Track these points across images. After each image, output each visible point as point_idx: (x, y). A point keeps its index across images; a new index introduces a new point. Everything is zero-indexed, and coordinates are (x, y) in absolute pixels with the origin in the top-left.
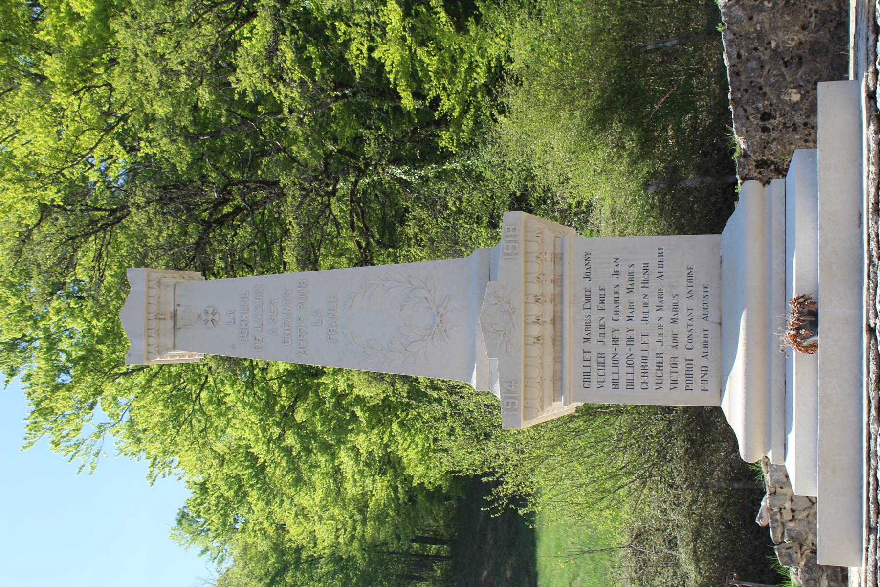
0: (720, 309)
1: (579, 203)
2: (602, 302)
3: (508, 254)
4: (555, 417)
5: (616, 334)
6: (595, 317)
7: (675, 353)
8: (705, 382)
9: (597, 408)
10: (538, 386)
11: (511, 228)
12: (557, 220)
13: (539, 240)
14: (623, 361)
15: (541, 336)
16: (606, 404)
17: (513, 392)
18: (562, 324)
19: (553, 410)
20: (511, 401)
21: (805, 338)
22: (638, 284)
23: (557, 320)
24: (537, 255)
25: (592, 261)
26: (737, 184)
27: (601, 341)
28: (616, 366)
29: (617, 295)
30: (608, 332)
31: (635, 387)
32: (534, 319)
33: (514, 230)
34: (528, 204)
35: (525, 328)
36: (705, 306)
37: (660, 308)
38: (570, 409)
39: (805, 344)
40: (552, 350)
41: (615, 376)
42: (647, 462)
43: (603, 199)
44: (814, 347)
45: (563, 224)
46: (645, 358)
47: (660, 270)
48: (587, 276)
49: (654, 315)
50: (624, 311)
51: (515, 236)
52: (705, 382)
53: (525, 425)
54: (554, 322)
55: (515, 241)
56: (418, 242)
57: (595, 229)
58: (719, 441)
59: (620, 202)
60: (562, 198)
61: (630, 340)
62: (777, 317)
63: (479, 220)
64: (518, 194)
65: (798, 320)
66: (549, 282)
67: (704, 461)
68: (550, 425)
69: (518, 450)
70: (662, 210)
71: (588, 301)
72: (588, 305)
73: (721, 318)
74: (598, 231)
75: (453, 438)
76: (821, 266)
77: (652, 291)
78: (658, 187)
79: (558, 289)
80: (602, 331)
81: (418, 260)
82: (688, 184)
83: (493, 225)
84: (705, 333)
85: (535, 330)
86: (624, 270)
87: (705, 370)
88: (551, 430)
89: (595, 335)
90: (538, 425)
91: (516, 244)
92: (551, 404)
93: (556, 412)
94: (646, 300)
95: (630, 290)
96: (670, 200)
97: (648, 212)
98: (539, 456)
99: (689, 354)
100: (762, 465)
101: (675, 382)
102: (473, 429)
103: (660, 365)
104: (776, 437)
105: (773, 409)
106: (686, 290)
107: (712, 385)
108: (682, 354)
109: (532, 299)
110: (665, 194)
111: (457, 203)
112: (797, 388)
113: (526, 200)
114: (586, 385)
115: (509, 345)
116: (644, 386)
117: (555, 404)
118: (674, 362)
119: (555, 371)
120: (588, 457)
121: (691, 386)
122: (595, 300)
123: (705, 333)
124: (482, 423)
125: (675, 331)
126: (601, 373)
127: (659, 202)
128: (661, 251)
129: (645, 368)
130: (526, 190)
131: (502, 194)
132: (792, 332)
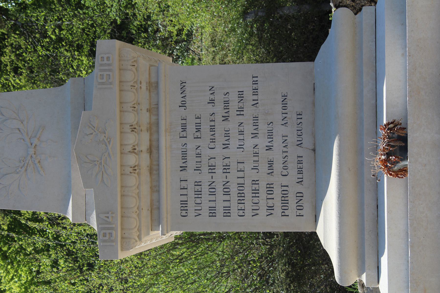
0: (314, 135)
1: (180, 32)
2: (198, 130)
3: (103, 83)
4: (158, 245)
5: (212, 162)
6: (191, 145)
7: (271, 179)
8: (300, 208)
9: (200, 235)
10: (135, 216)
11: (105, 56)
12: (158, 49)
13: (134, 69)
14: (220, 189)
15: (138, 165)
16: (209, 231)
17: (110, 223)
18: (158, 153)
19: (152, 240)
20: (107, 232)
21: (394, 163)
22: (233, 112)
23: (153, 149)
24: (132, 83)
25: (188, 89)
26: (331, 12)
27: (198, 169)
28: (212, 194)
29: (212, 123)
30: (205, 160)
31: (232, 214)
32: (130, 148)
33: (108, 58)
34: (129, 33)
35: (121, 158)
36: (299, 133)
37: (255, 136)
38: (170, 237)
39: (396, 168)
40: (149, 179)
41: (212, 204)
42: (250, 286)
43: (203, 27)
44: (404, 171)
45: (165, 53)
46: (241, 185)
47: (255, 97)
48: (183, 105)
49: (249, 143)
50: (220, 139)
51: (109, 65)
52: (300, 208)
53: (122, 255)
54: (150, 151)
55: (110, 70)
56: (16, 70)
57: (197, 58)
58: (319, 264)
59: (220, 29)
60: (163, 26)
61: (226, 168)
62: (368, 143)
63: (79, 48)
64: (119, 22)
65: (388, 145)
66: (144, 111)
67: (305, 283)
68: (153, 253)
69: (122, 279)
70: (260, 38)
71: (184, 130)
72: (184, 134)
73: (314, 144)
74: (200, 59)
75: (55, 270)
76: (410, 92)
77: (247, 118)
78: (256, 15)
79: (154, 118)
80: (199, 159)
81: (18, 89)
82: (286, 12)
83: (92, 54)
84: (300, 159)
85: (132, 160)
86: (219, 98)
87: (300, 196)
88: (155, 258)
89: (191, 163)
90: (141, 254)
91: (110, 73)
92: (148, 234)
93: (154, 241)
94: (241, 128)
95: (226, 118)
96: (269, 28)
97: (247, 40)
98: (142, 285)
99: (285, 181)
100: (359, 287)
101: (271, 208)
102: (75, 260)
103: (256, 192)
104: (370, 261)
105: (366, 233)
106: (280, 117)
107: (307, 211)
108: (277, 180)
109: (127, 129)
110: (264, 22)
111: (57, 31)
112: (388, 212)
113: (127, 28)
114: (184, 213)
115: (105, 175)
116: (241, 213)
117: (153, 233)
118: (270, 188)
119: (152, 201)
120: (192, 284)
121: (287, 212)
122: (191, 128)
123: (300, 159)
124: (85, 254)
125: (271, 158)
126: (198, 201)
127: (257, 30)
128: (255, 79)
129: (241, 195)
130: (127, 18)
131: (102, 21)
132: (383, 157)
